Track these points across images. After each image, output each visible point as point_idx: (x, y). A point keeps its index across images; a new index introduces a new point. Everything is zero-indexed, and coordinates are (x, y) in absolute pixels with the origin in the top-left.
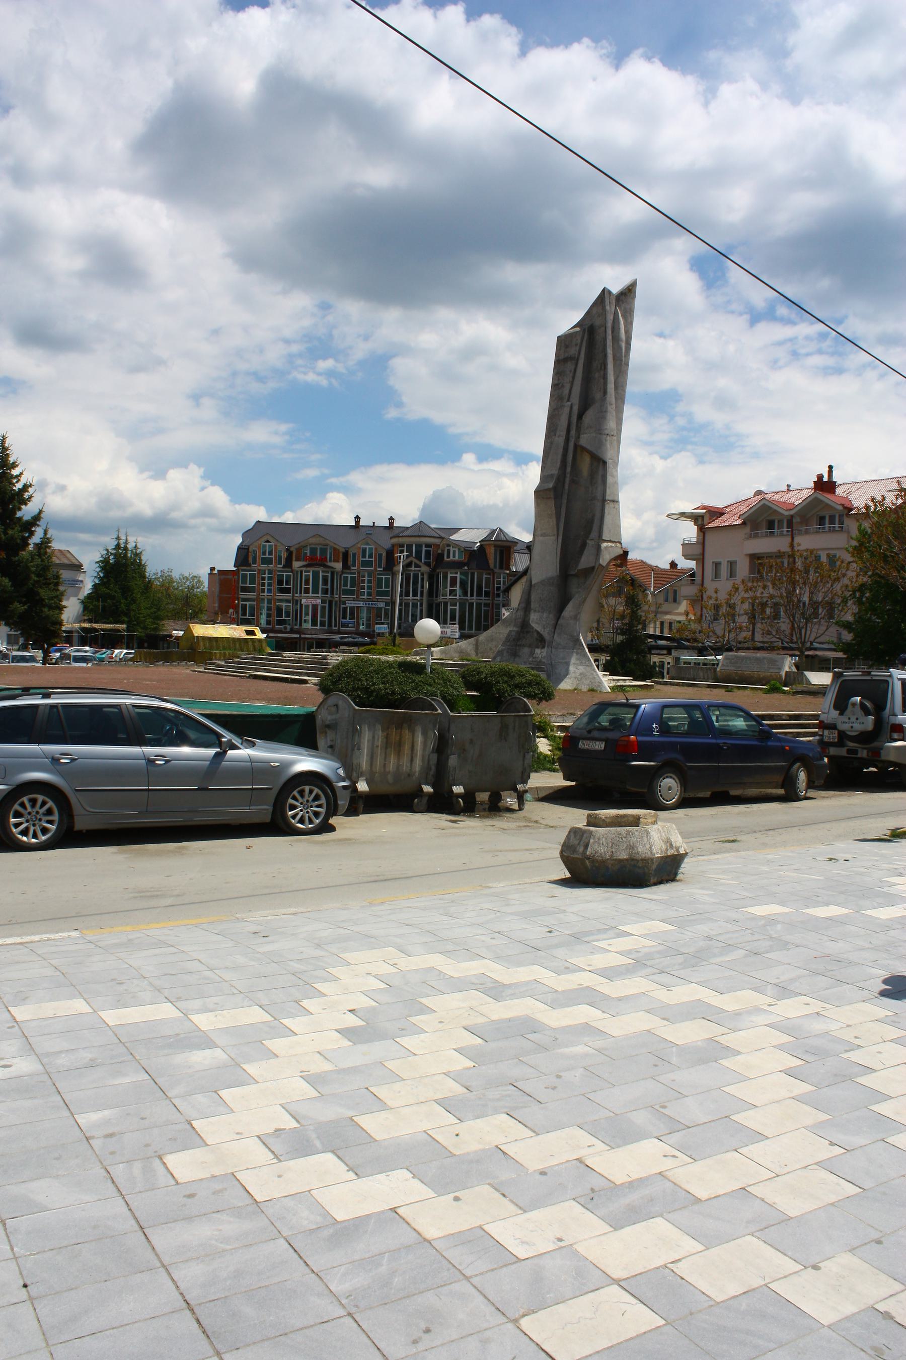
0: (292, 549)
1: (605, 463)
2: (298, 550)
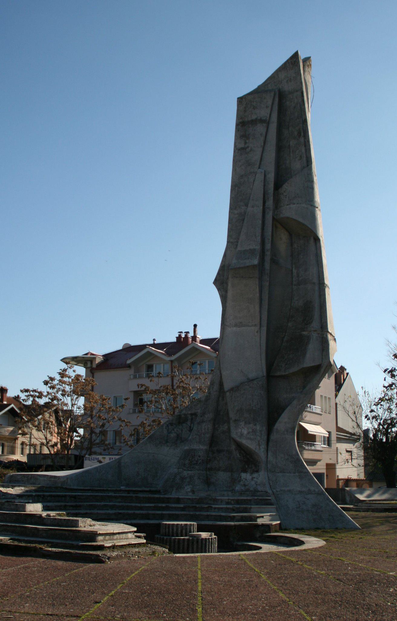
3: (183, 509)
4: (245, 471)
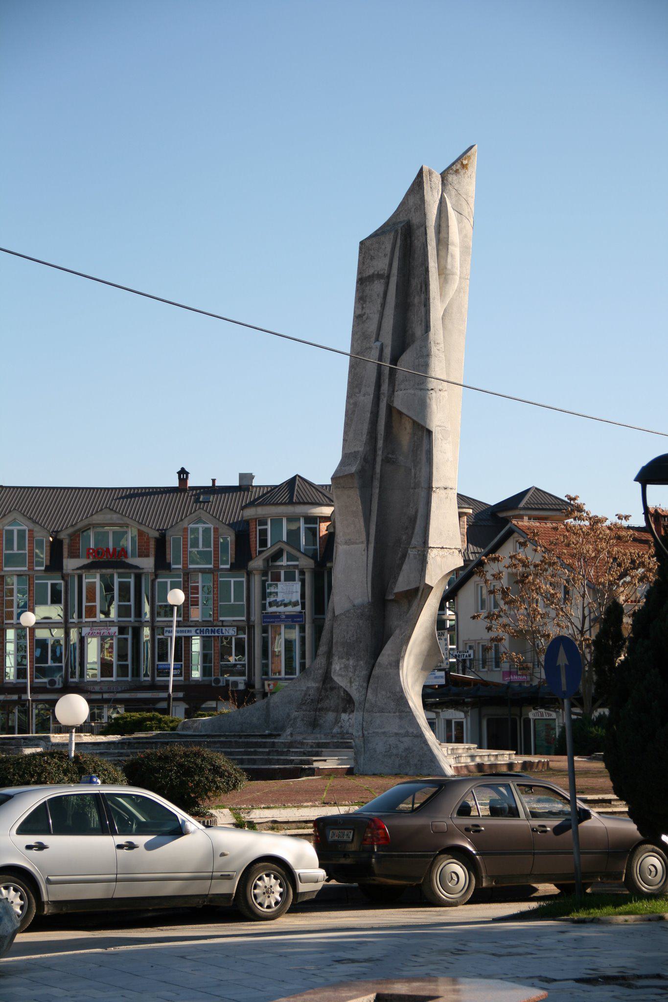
0: (63, 536)
1: (430, 433)
2: (75, 537)
3: (268, 753)
4: (345, 711)
